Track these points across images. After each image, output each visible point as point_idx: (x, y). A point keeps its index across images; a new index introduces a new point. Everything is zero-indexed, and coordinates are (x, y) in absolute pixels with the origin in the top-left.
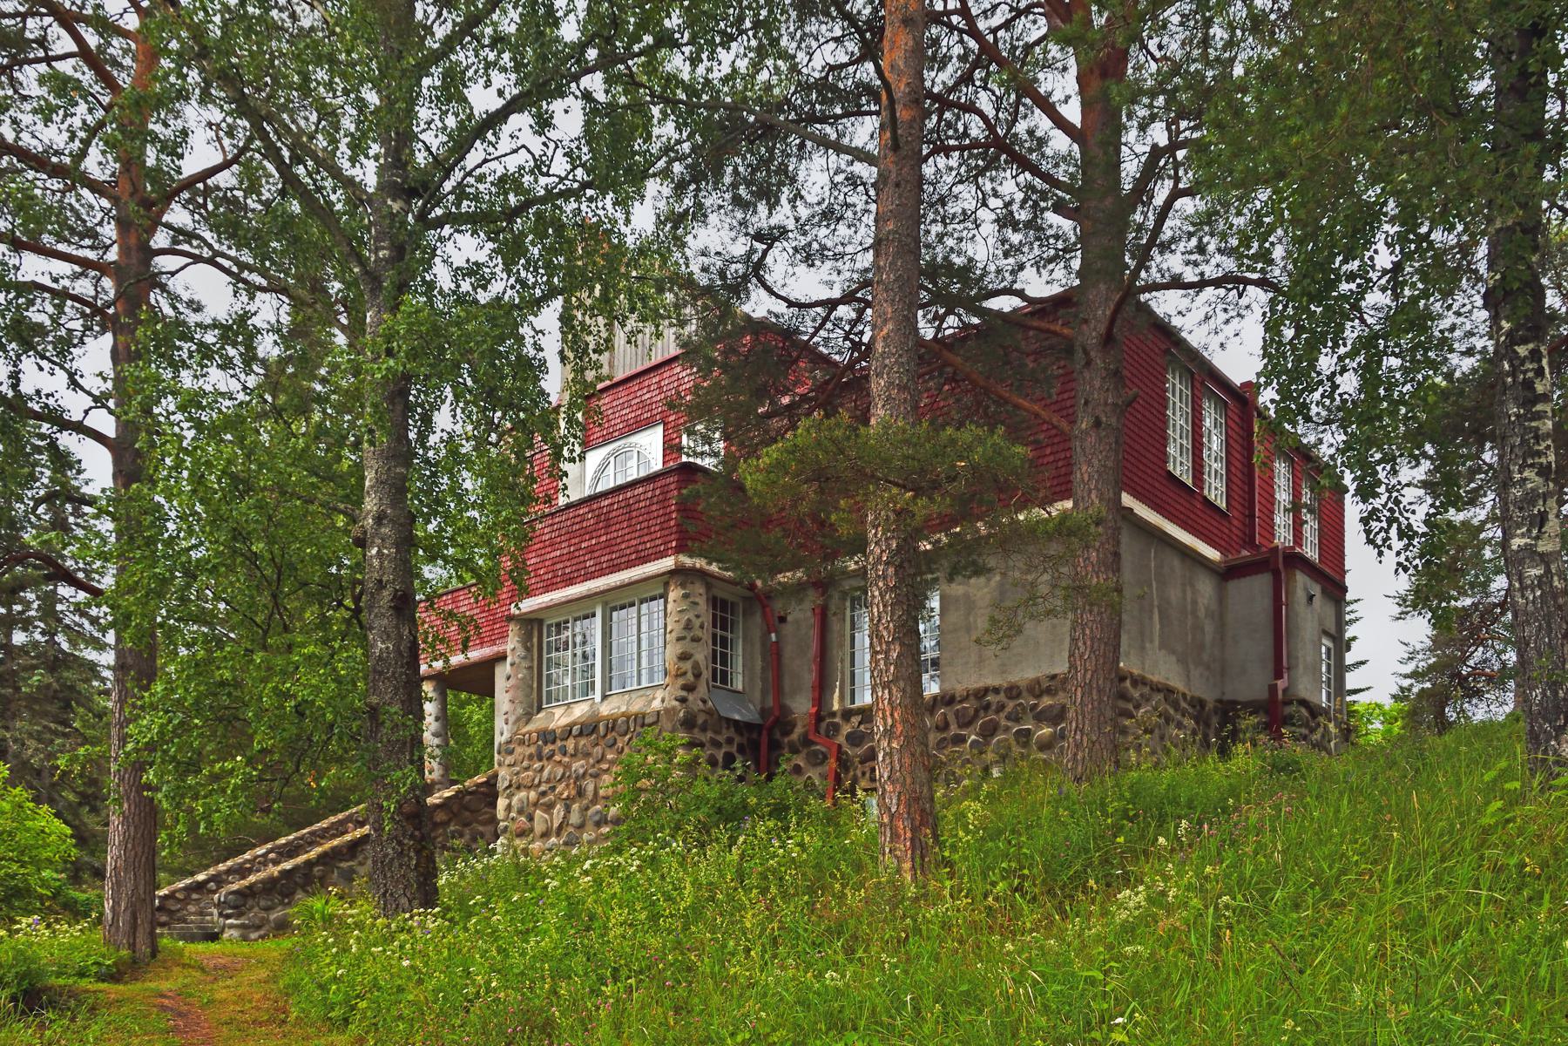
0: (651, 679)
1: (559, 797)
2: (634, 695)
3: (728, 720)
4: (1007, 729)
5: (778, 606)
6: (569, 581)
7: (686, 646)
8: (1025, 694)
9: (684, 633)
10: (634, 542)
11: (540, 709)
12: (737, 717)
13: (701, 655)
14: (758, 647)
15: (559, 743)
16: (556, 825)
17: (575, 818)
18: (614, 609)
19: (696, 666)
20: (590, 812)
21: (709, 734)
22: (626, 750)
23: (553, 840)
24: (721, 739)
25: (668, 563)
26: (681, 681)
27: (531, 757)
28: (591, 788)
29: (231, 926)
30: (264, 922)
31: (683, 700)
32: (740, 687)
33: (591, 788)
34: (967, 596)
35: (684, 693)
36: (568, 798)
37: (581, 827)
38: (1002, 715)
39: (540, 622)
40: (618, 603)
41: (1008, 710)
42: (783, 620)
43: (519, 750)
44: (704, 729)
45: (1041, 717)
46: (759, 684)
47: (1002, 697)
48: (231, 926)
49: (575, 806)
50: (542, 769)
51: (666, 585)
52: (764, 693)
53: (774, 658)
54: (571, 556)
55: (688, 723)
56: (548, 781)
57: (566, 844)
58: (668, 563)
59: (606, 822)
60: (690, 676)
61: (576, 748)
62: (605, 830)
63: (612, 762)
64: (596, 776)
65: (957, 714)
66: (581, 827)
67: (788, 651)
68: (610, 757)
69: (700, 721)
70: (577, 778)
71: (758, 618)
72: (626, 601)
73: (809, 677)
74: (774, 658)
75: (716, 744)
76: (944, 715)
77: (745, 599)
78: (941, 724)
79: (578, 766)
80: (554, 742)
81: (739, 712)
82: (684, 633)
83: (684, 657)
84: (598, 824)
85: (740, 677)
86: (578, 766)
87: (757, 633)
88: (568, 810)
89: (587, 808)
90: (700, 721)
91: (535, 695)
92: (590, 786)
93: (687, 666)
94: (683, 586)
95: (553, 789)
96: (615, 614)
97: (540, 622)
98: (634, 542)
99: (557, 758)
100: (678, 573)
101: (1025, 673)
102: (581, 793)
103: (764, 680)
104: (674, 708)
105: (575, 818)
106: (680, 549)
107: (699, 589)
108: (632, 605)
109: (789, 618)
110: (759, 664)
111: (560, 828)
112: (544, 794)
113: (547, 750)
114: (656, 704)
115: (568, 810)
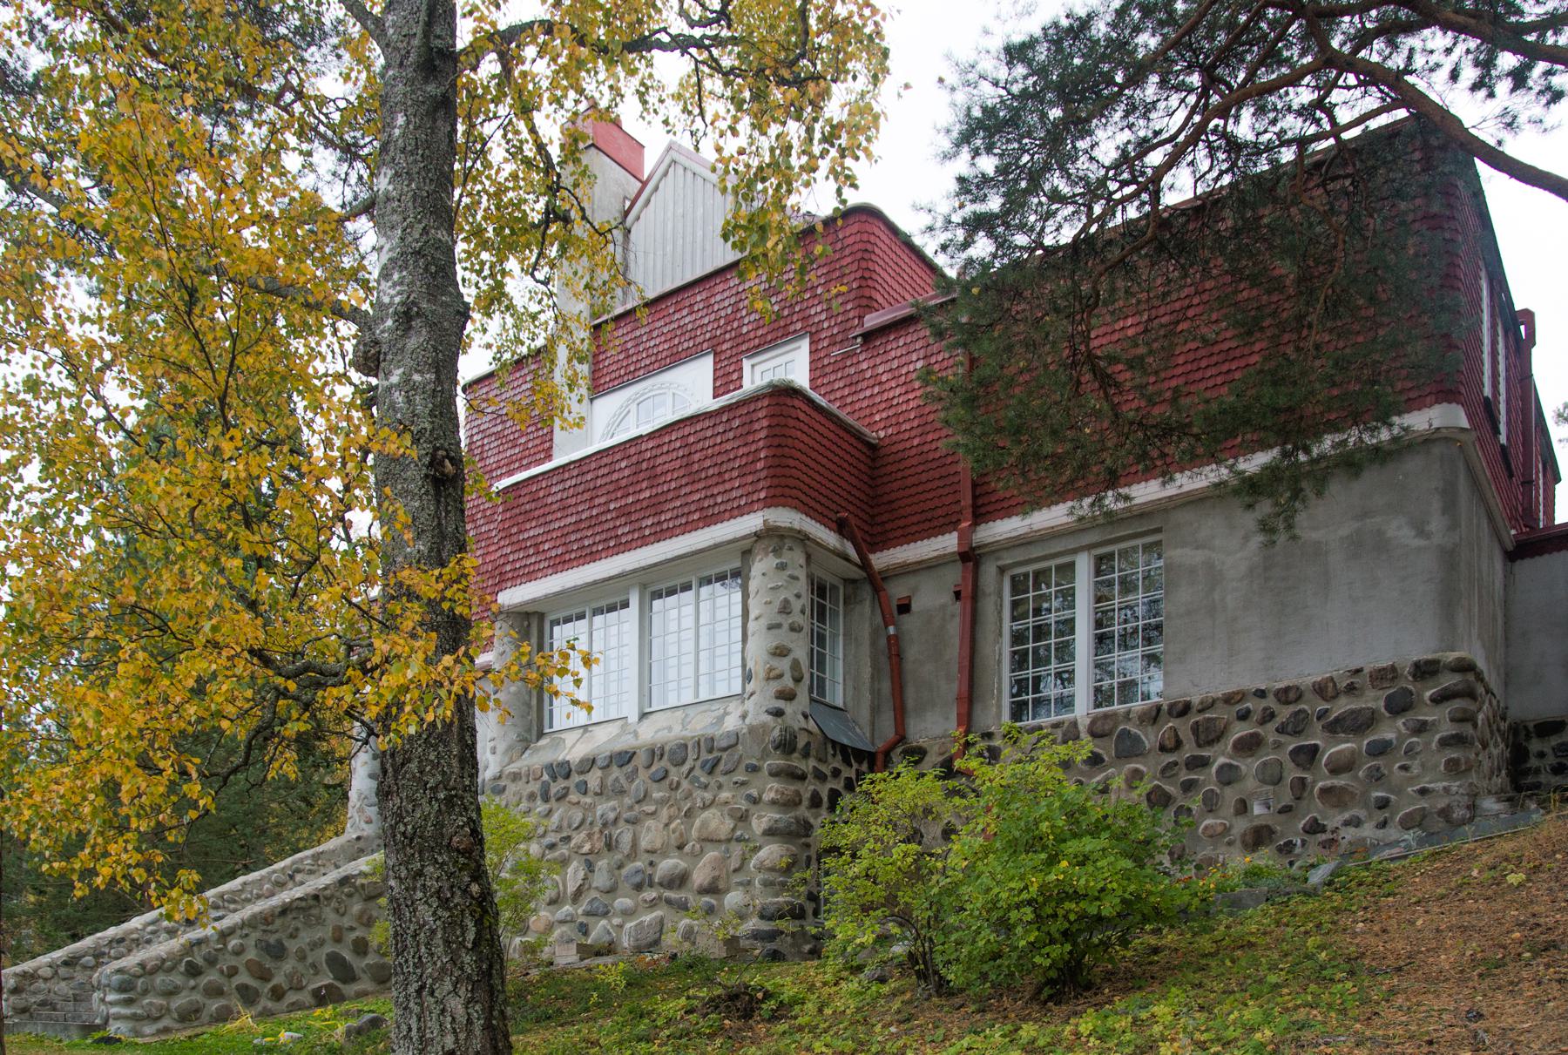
0: (713, 688)
1: (577, 850)
2: (691, 711)
3: (834, 743)
4: (1278, 746)
5: (897, 590)
6: (592, 556)
7: (783, 637)
8: (1308, 696)
9: (779, 619)
10: (696, 497)
11: (541, 735)
12: (845, 741)
13: (800, 652)
14: (866, 649)
15: (576, 778)
16: (571, 888)
17: (601, 879)
18: (658, 595)
19: (796, 665)
20: (624, 871)
21: (812, 762)
22: (685, 784)
23: (567, 908)
24: (824, 769)
25: (751, 523)
26: (775, 686)
27: (532, 797)
28: (626, 839)
29: (118, 1017)
30: (164, 1012)
31: (778, 713)
32: (839, 703)
33: (626, 839)
34: (1209, 565)
35: (780, 704)
36: (591, 852)
37: (611, 891)
38: (1272, 726)
39: (541, 616)
40: (663, 586)
41: (1278, 720)
42: (905, 608)
43: (512, 788)
44: (806, 755)
45: (1335, 727)
46: (867, 697)
47: (1270, 702)
48: (118, 1017)
49: (602, 864)
50: (549, 813)
51: (747, 554)
52: (875, 710)
53: (893, 657)
54: (594, 522)
55: (786, 745)
56: (559, 829)
57: (587, 914)
58: (751, 523)
59: (651, 885)
60: (788, 682)
61: (602, 785)
62: (650, 894)
63: (662, 802)
64: (633, 822)
65: (1195, 729)
66: (611, 891)
67: (913, 653)
68: (656, 795)
69: (801, 744)
70: (605, 825)
71: (866, 607)
72: (678, 582)
73: (951, 688)
74: (893, 657)
75: (820, 777)
76: (1174, 730)
77: (848, 581)
78: (1170, 744)
79: (605, 808)
80: (567, 776)
81: (849, 737)
82: (779, 619)
83: (780, 652)
84: (639, 887)
85: (840, 688)
86: (605, 808)
87: (865, 632)
88: (590, 867)
89: (620, 867)
90: (801, 744)
91: (534, 715)
92: (625, 835)
93: (784, 665)
94: (777, 552)
95: (568, 839)
96: (657, 604)
97: (541, 616)
98: (696, 497)
99: (573, 797)
100: (771, 537)
101: (1306, 668)
102: (610, 846)
103: (876, 693)
104: (764, 726)
105: (601, 879)
106: (771, 502)
107: (796, 557)
108: (581, 617)
109: (914, 607)
110: (867, 672)
111: (578, 893)
112: (552, 846)
113: (555, 788)
114: (732, 723)
115: (590, 867)
